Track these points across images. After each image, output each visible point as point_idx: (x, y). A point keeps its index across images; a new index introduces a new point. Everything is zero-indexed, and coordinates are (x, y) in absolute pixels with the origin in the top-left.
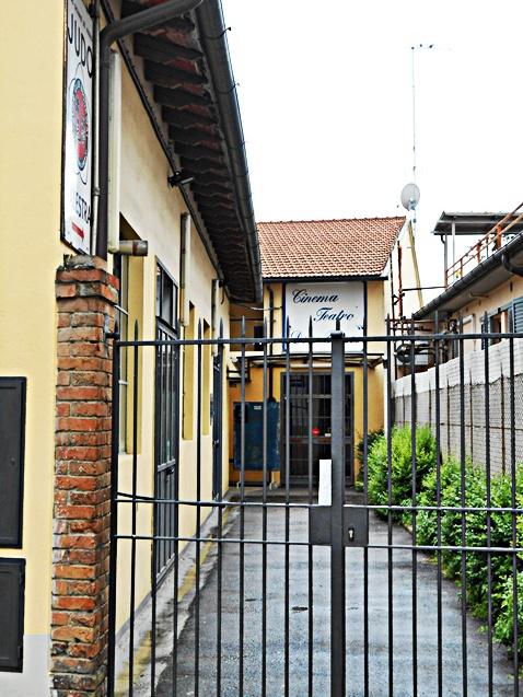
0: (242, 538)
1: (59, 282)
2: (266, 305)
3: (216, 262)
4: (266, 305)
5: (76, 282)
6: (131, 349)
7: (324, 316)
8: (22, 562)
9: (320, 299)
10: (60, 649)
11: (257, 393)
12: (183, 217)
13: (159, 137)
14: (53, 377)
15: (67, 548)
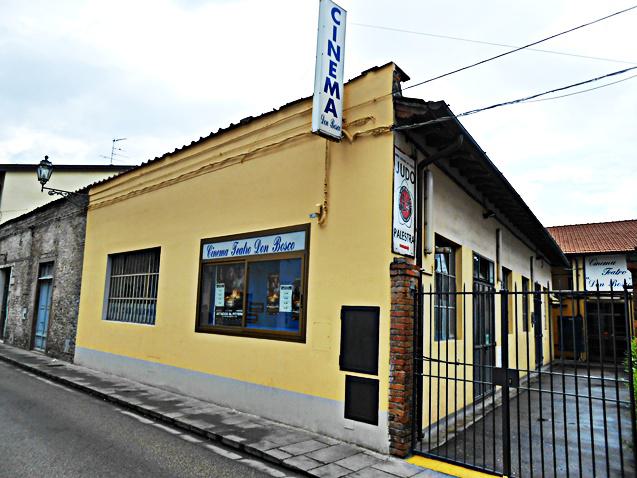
0: (529, 387)
1: (391, 269)
2: (574, 267)
3: (535, 248)
4: (574, 267)
5: (397, 269)
6: (433, 291)
7: (608, 272)
8: (377, 381)
9: (605, 264)
10: (391, 418)
11: (570, 312)
12: (498, 231)
13: (474, 198)
14: (389, 307)
15: (394, 377)
